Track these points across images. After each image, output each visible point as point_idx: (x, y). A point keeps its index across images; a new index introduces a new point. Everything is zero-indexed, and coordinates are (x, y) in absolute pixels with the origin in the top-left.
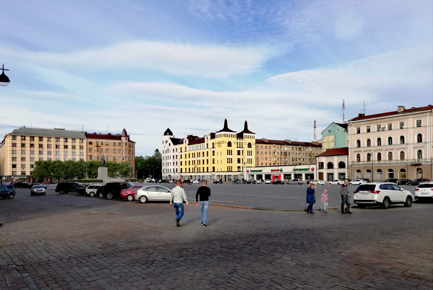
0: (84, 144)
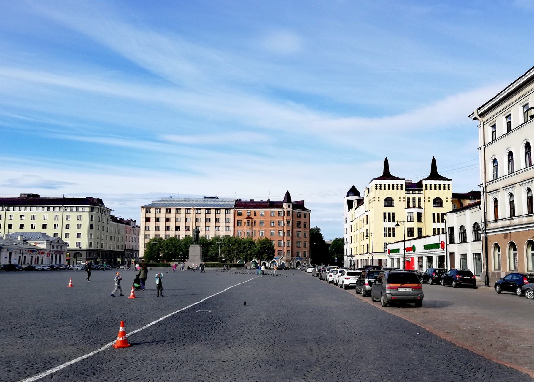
0: (231, 216)
